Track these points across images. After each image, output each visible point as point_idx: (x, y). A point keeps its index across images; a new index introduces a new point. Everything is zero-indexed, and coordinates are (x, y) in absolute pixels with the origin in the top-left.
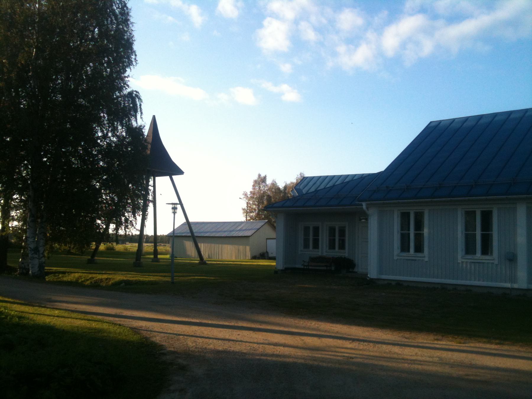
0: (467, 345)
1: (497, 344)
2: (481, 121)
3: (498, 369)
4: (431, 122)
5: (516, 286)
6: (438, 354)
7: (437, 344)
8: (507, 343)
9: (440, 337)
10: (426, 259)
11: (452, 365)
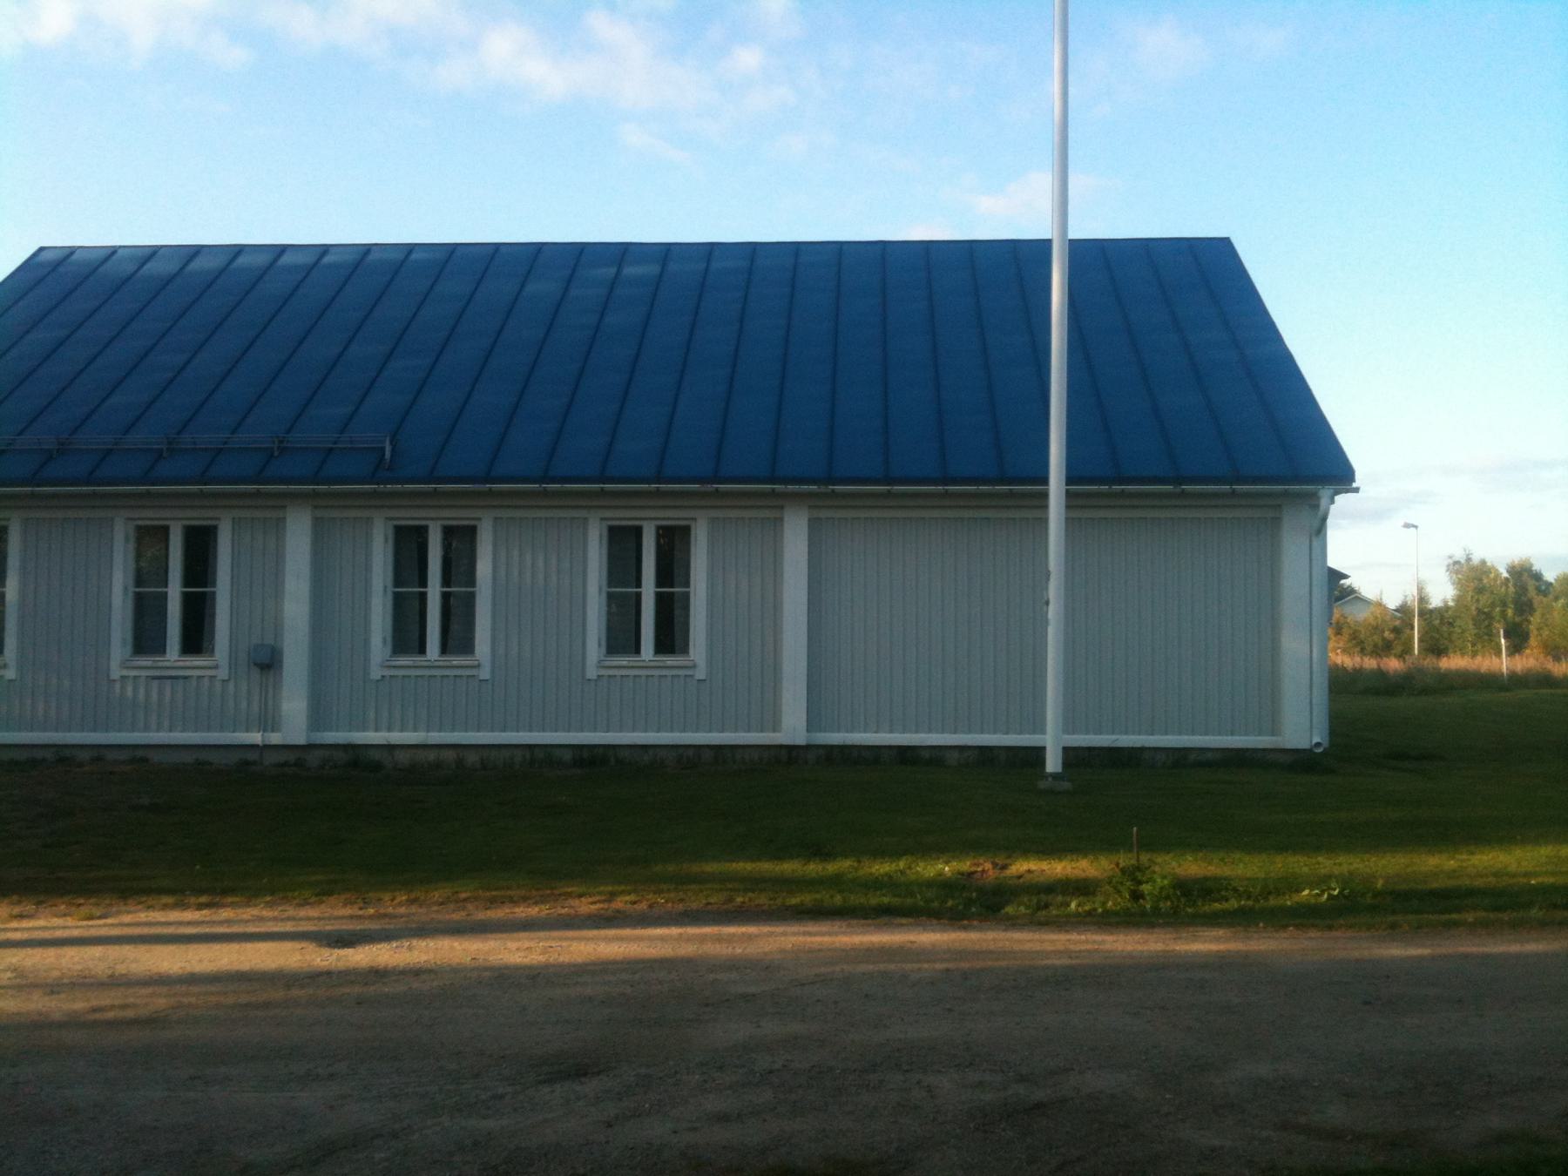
0: (109, 921)
1: (200, 907)
2: (196, 265)
3: (192, 979)
4: (42, 249)
5: (275, 738)
6: (14, 960)
7: (16, 930)
8: (230, 900)
9: (30, 908)
10: (701, 674)
11: (54, 988)
